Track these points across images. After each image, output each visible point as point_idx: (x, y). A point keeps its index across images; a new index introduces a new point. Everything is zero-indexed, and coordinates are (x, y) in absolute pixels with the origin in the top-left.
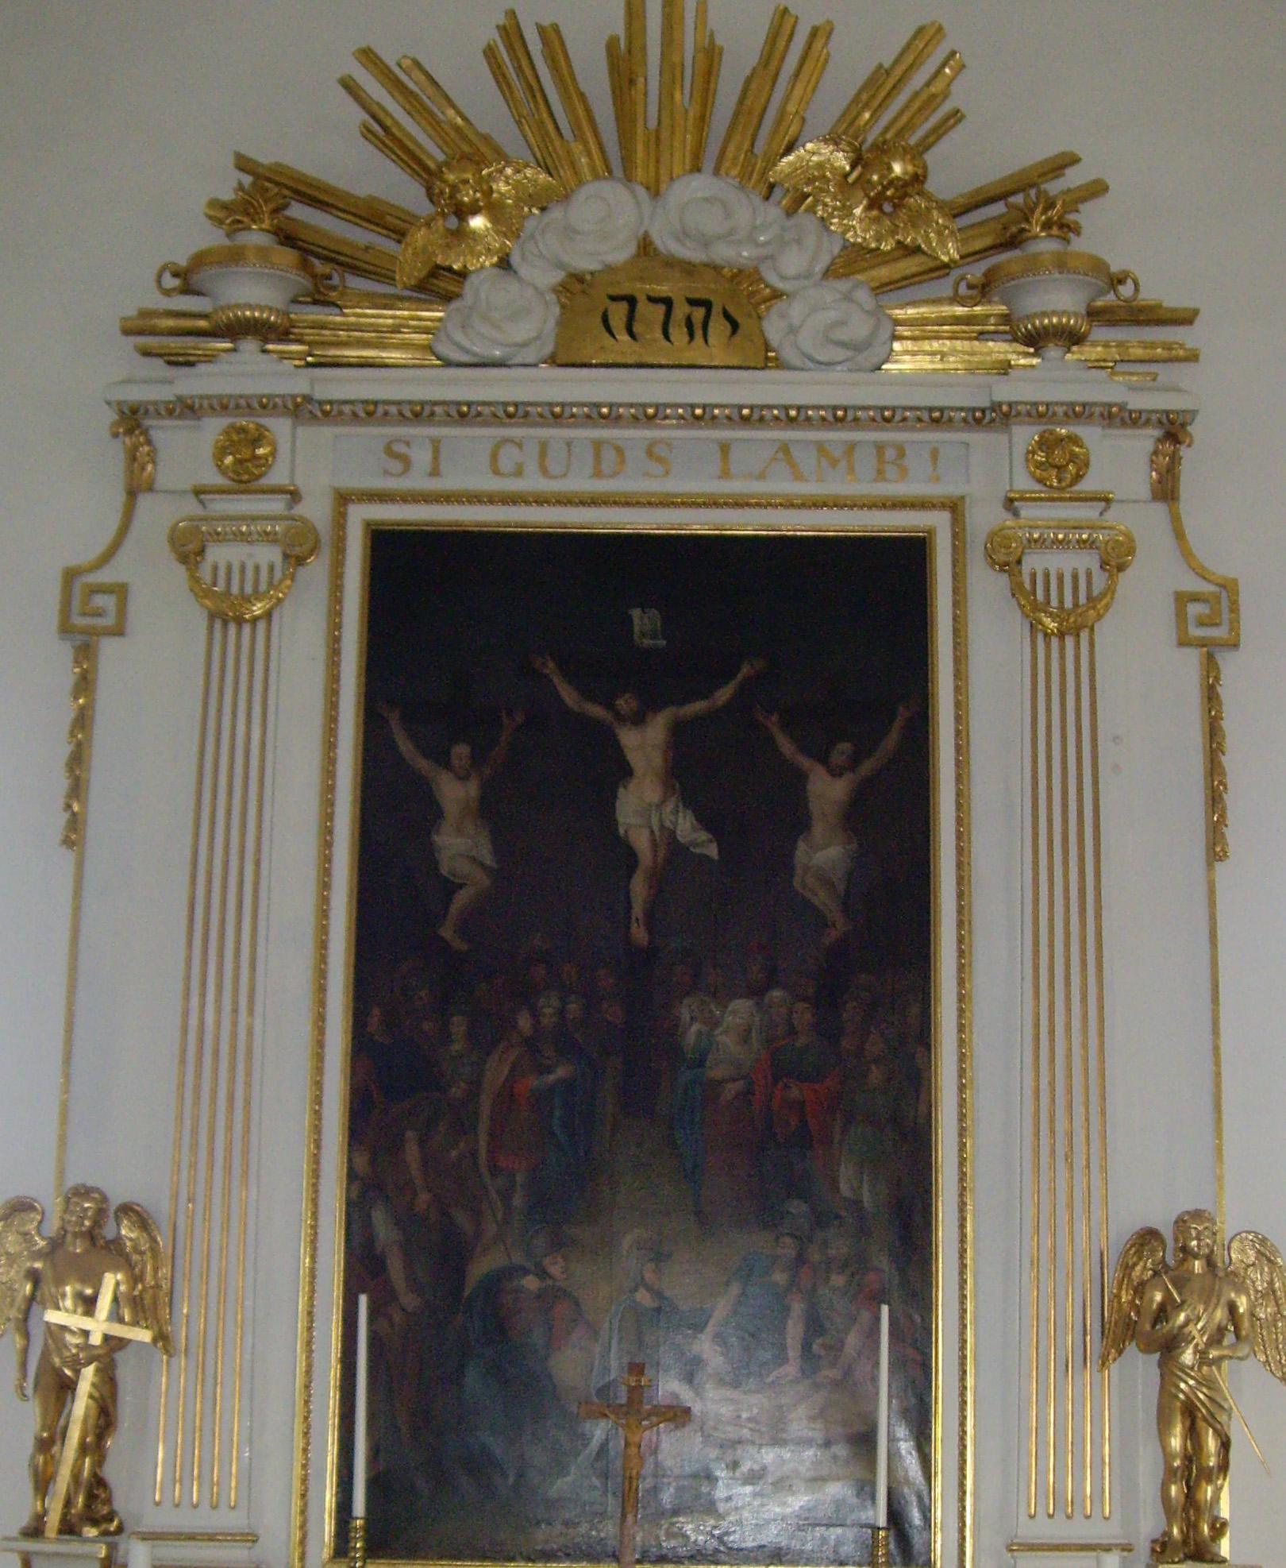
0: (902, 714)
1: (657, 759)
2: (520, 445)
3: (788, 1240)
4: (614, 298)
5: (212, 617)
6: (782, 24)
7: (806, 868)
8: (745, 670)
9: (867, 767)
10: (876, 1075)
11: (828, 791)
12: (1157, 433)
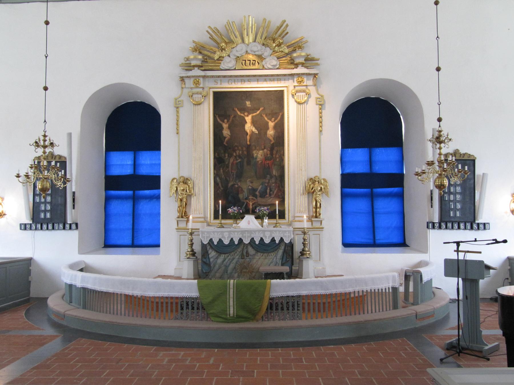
1: (250, 121)
9: (276, 121)
10: (278, 160)
11: (271, 124)
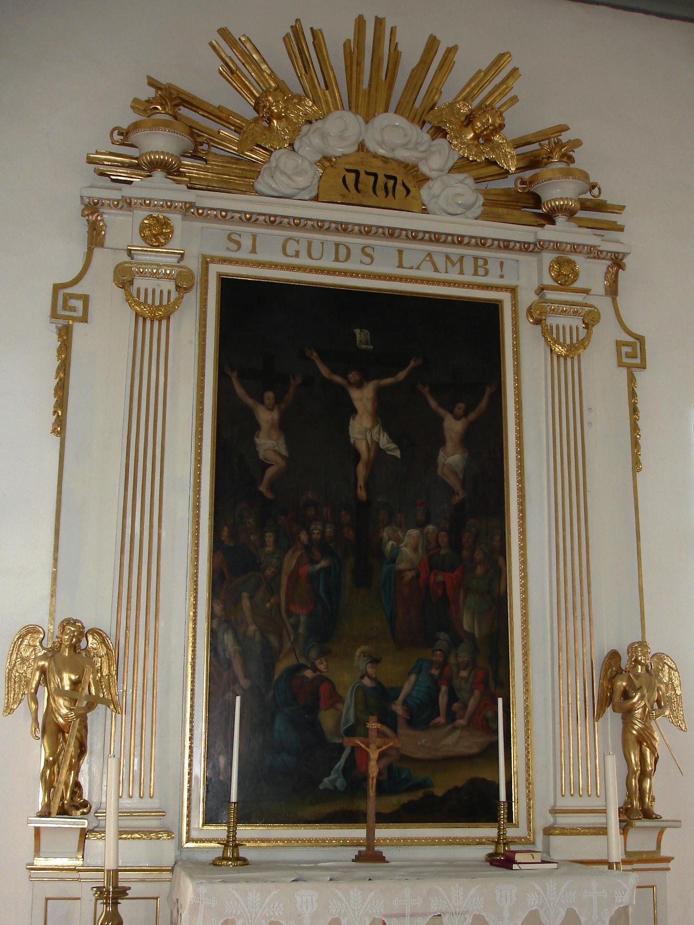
0: (488, 391)
1: (369, 406)
2: (298, 242)
3: (438, 653)
4: (348, 171)
5: (137, 315)
6: (432, 43)
7: (444, 465)
8: (412, 363)
9: (472, 416)
10: (479, 571)
11: (453, 427)
12: (609, 263)
